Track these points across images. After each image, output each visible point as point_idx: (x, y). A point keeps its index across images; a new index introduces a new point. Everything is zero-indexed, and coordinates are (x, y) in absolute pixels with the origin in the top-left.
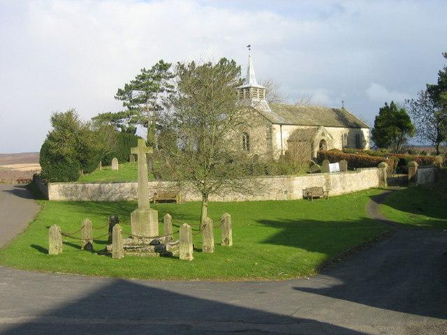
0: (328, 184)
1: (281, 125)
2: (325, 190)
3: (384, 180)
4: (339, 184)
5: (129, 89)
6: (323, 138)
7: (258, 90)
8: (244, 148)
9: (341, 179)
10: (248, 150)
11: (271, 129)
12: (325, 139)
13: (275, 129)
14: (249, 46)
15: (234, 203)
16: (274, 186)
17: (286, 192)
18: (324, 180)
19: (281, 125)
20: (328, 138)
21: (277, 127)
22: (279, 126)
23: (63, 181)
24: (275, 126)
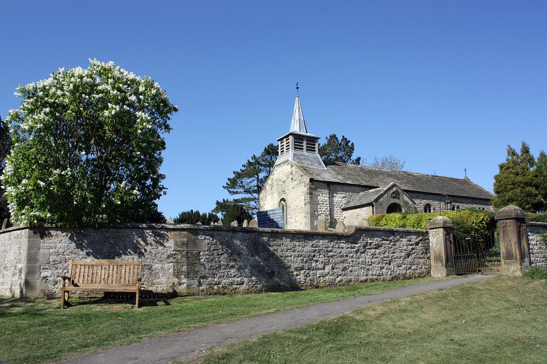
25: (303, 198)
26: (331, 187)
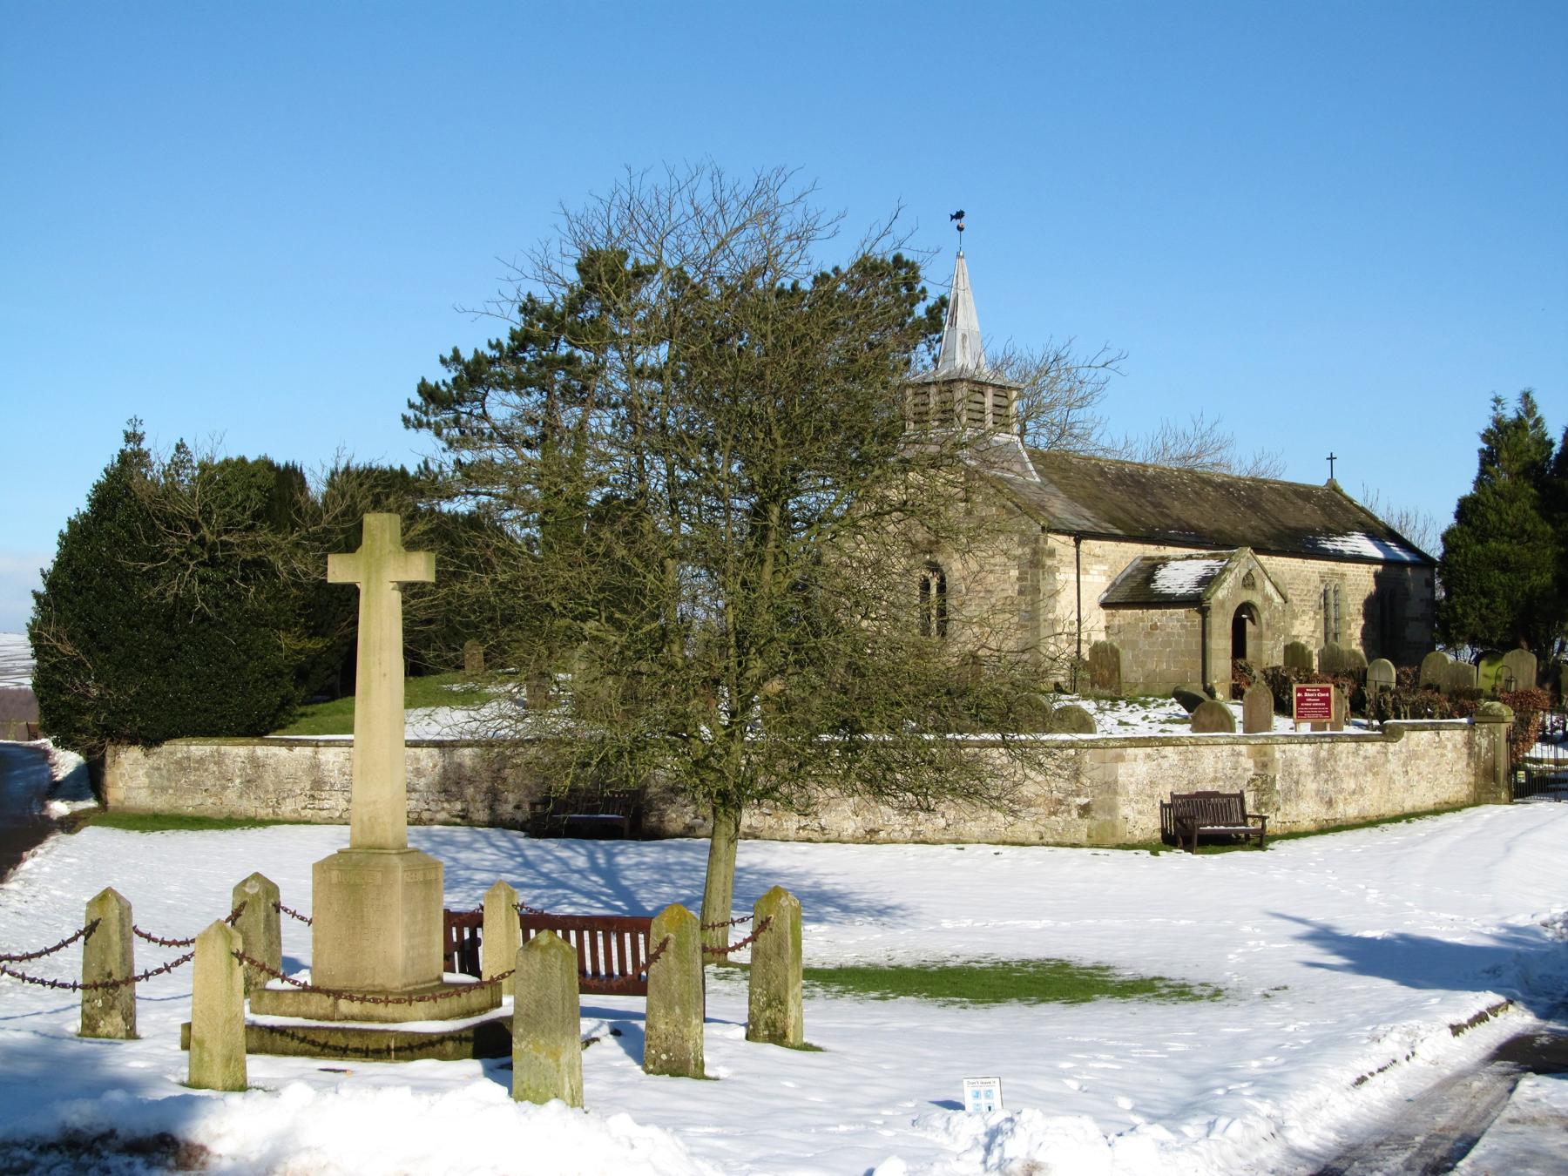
0: (1263, 783)
1: (1079, 536)
2: (1249, 810)
3: (1495, 778)
4: (1310, 786)
5: (474, 376)
6: (1247, 596)
7: (990, 392)
8: (925, 631)
9: (1319, 765)
10: (943, 633)
11: (1035, 552)
12: (1256, 599)
13: (1052, 553)
14: (959, 215)
15: (1365, 616)
16: (1028, 790)
17: (1085, 810)
18: (1250, 764)
19: (1079, 536)
20: (1268, 598)
21: (1061, 544)
22: (1071, 541)
23: (944, 995)
24: (1055, 541)
25: (1014, 573)
26: (1088, 545)
